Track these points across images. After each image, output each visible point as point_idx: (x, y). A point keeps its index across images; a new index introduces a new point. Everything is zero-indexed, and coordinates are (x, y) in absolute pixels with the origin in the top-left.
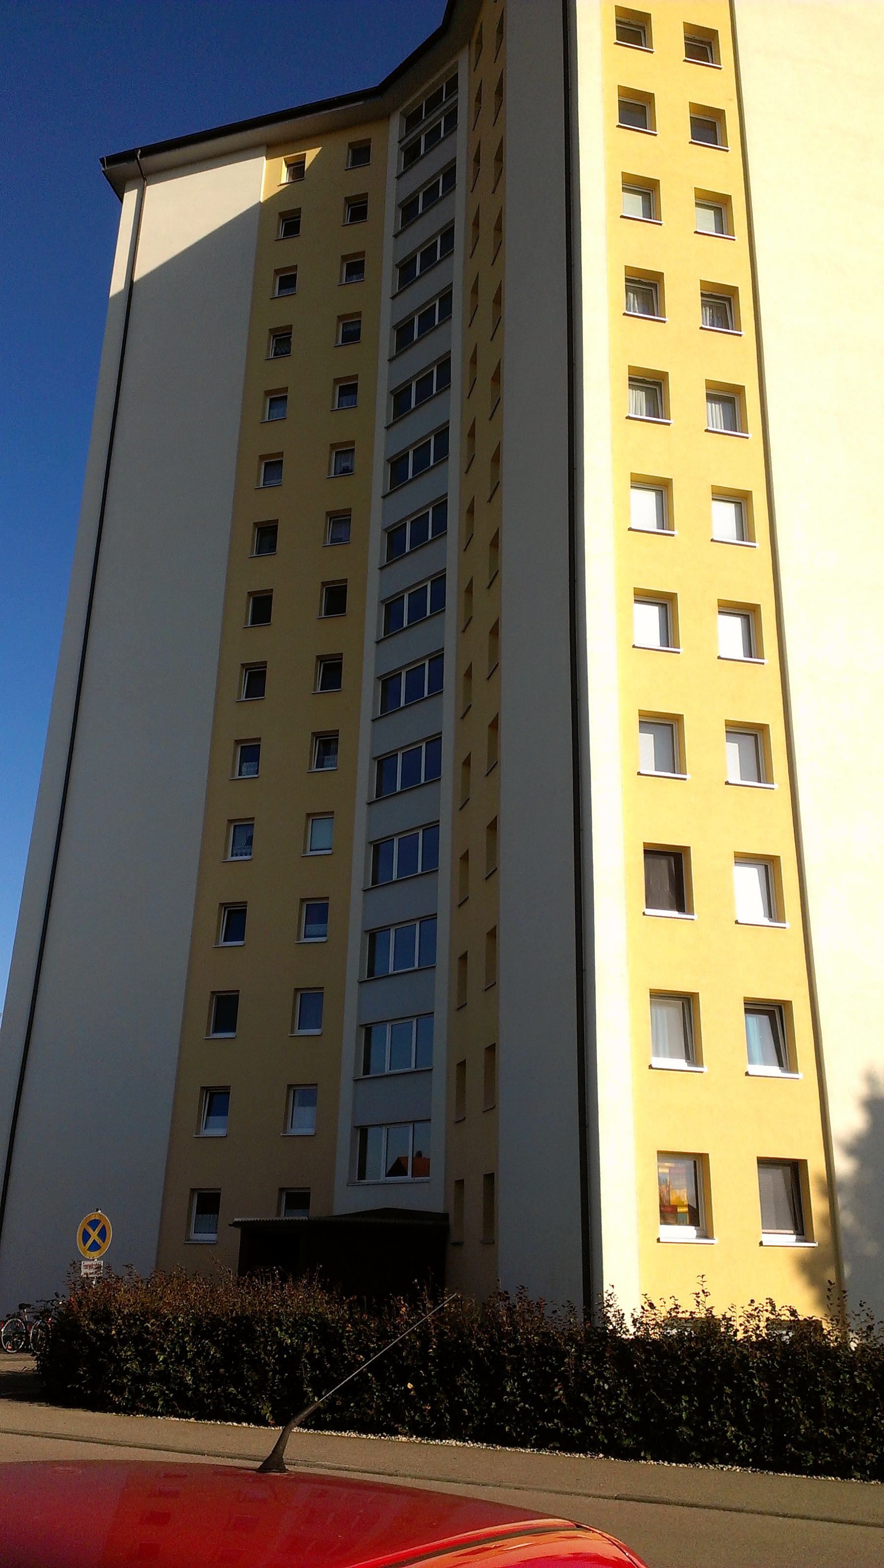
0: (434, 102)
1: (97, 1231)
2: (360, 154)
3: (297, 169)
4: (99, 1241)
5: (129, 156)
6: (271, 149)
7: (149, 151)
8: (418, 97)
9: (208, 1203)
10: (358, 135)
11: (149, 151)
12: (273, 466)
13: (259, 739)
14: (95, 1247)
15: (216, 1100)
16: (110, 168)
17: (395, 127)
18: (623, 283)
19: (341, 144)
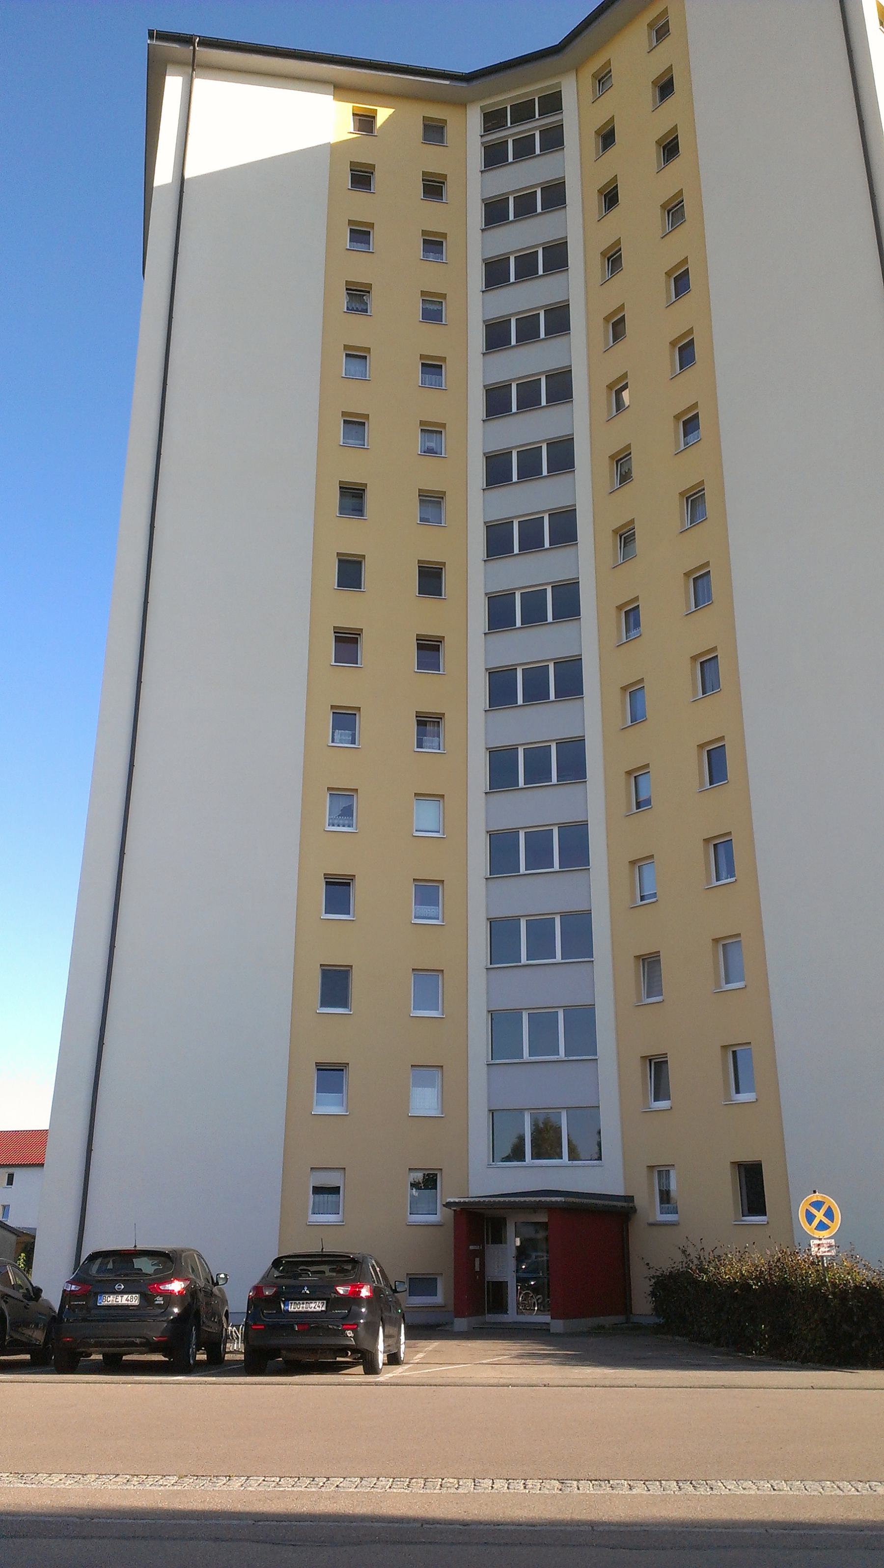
0: (523, 112)
1: (823, 1211)
2: (434, 132)
3: (365, 122)
4: (826, 1221)
5: (186, 40)
6: (341, 90)
7: (208, 43)
8: (505, 98)
9: (430, 1182)
10: (435, 112)
11: (208, 43)
12: (355, 425)
13: (722, 738)
14: (822, 1226)
15: (331, 1074)
16: (159, 43)
17: (474, 119)
18: (345, 292)
19: (416, 115)
